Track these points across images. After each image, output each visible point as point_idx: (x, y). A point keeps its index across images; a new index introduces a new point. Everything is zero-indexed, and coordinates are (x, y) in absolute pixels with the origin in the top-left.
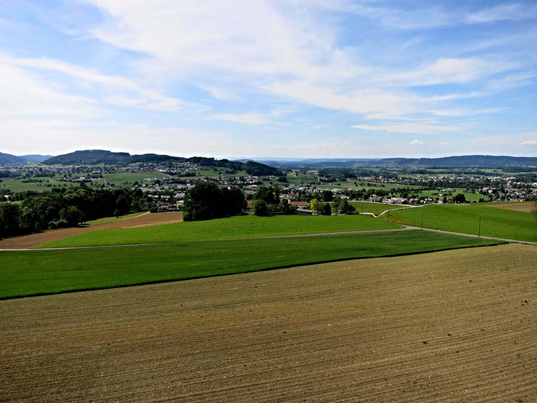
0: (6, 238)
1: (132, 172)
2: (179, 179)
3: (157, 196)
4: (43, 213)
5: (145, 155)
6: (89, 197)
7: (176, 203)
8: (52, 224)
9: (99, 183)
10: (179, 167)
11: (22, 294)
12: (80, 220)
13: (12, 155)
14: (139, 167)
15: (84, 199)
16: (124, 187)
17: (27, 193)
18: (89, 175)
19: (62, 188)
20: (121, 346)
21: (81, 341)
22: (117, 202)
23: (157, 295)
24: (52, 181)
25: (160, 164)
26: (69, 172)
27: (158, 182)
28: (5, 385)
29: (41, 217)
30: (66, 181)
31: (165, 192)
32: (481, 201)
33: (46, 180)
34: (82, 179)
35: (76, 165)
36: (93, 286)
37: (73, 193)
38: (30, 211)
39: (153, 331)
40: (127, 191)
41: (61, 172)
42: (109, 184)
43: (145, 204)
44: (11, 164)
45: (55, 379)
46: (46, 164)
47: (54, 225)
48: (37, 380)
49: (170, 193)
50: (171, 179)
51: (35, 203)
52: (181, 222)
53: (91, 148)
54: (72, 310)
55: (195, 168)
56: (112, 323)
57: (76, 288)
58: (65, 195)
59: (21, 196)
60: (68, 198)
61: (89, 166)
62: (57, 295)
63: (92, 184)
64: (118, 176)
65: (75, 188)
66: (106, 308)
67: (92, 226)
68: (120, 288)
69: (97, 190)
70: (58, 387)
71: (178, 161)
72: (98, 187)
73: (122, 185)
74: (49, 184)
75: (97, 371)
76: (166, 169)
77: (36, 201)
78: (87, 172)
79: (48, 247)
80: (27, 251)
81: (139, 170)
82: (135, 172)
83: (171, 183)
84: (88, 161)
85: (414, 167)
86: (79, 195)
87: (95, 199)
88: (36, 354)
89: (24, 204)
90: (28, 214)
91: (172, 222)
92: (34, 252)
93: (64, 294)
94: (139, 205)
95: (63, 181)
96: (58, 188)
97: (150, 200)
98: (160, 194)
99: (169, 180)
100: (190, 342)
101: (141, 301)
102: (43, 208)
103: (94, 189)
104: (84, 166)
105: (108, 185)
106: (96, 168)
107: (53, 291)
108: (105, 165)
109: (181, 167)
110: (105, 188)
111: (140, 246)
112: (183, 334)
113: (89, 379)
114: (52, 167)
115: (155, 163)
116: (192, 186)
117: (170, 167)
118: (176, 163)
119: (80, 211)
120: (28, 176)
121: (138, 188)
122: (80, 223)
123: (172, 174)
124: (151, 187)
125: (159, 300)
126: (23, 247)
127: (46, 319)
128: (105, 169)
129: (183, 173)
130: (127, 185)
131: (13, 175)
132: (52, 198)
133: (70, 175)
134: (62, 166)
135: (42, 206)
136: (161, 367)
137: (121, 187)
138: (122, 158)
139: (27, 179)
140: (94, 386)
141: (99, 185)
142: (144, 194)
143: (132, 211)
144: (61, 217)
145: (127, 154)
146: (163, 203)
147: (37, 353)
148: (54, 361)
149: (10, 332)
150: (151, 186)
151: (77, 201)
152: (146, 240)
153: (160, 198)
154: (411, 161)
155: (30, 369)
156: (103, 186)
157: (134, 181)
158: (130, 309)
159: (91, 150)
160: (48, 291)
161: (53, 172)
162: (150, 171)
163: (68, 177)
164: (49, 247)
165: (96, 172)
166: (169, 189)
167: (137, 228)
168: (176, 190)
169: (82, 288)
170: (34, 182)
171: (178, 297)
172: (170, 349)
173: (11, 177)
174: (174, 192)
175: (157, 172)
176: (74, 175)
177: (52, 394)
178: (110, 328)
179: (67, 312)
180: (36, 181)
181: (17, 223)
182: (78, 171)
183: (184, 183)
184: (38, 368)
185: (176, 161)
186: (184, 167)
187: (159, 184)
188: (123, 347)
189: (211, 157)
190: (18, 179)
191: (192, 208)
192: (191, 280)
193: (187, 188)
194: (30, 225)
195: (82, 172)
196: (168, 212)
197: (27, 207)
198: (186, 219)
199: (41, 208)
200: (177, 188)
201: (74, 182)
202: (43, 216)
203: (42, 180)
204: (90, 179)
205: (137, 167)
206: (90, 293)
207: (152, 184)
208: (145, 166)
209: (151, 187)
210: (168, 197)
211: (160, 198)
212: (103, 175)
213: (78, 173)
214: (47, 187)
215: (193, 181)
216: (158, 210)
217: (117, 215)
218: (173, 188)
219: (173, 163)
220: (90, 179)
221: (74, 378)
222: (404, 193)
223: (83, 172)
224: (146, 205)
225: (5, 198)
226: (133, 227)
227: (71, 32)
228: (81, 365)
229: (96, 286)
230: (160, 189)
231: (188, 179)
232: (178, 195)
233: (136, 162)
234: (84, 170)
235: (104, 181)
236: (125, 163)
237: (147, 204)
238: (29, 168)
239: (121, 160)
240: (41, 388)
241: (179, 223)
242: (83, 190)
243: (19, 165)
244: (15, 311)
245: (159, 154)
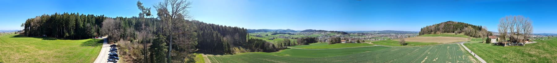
154: (376, 31)
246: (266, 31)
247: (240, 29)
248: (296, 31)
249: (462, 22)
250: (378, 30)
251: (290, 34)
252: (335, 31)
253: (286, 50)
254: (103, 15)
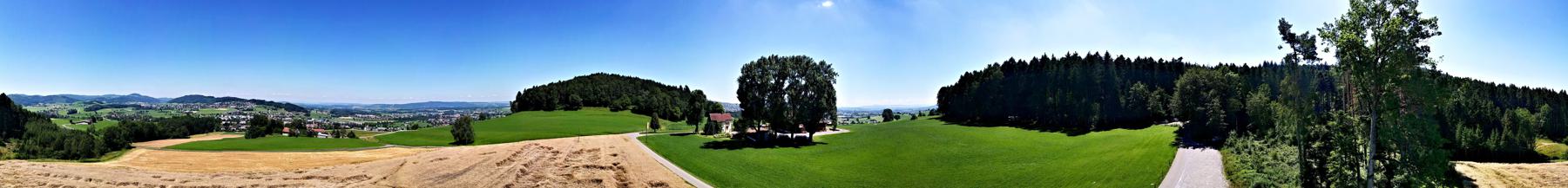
32: (428, 126)
55: (254, 106)
85: (390, 109)
154: (389, 106)
183: (246, 115)
222: (385, 125)
246: (69, 99)
247: (1554, 93)
248: (157, 101)
249: (633, 76)
250: (393, 103)
251: (139, 107)
252: (268, 100)
253: (805, 150)
254: (1181, 58)
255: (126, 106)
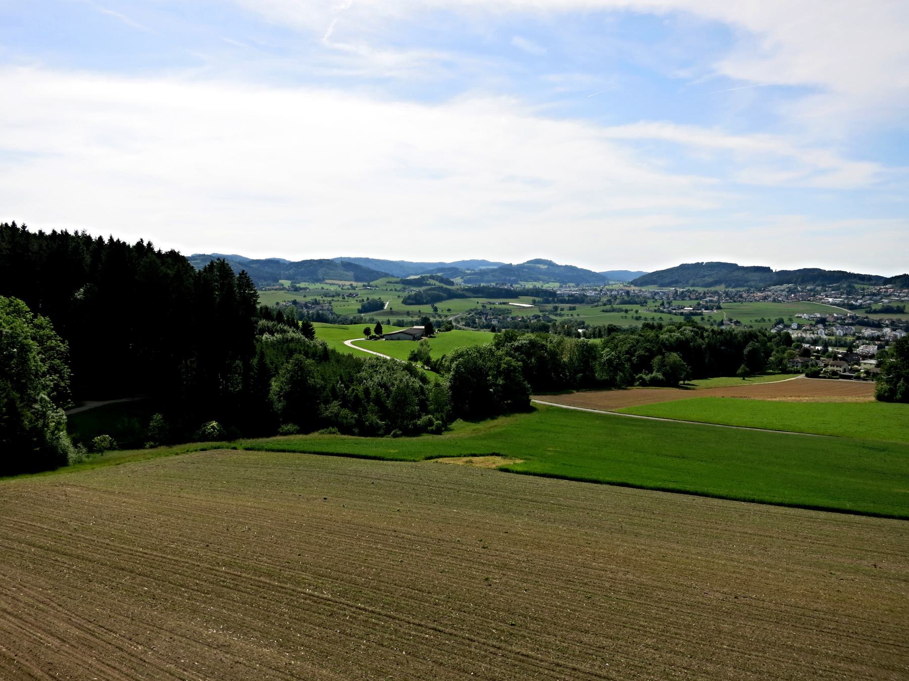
0: (578, 391)
1: (774, 301)
2: (867, 317)
3: (819, 348)
4: (629, 360)
5: (799, 271)
6: (700, 341)
7: (859, 364)
8: (641, 378)
9: (715, 318)
10: (869, 295)
11: (601, 478)
12: (682, 377)
13: (591, 271)
14: (788, 292)
15: (691, 344)
16: (756, 327)
17: (608, 328)
18: (699, 304)
19: (658, 324)
20: (758, 607)
21: (690, 578)
22: (746, 351)
23: (822, 532)
24: (643, 311)
25: (830, 287)
26: (668, 298)
27: (822, 321)
28: (582, 608)
29: (626, 366)
30: (662, 312)
31: (836, 341)
33: (634, 310)
34: (688, 309)
35: (680, 287)
36: (705, 490)
37: (674, 332)
38: (612, 356)
39: (818, 598)
40: (764, 335)
41: (657, 297)
42: (731, 320)
43: (795, 360)
44: (588, 284)
45: (651, 625)
46: (635, 285)
47: (644, 380)
48: (626, 617)
49: (845, 343)
50: (850, 317)
51: (619, 344)
52: (871, 402)
53: (705, 259)
54: (674, 521)
56: (739, 562)
57: (678, 488)
58: (662, 334)
59: (600, 331)
60: (667, 340)
61: (701, 290)
62: (649, 491)
63: (703, 319)
64: (747, 306)
65: (677, 325)
66: (729, 533)
67: (699, 389)
68: (752, 504)
69: (713, 331)
70: (655, 640)
71: (868, 283)
72: (712, 325)
73: (753, 323)
74: (638, 315)
75: (717, 637)
76: (840, 298)
77: (620, 341)
78: (697, 299)
79: (634, 413)
80: (605, 414)
81: (787, 298)
82: (780, 302)
83: (848, 324)
84: (698, 280)
86: (684, 335)
87: (709, 344)
88: (624, 577)
89: (603, 344)
90: (609, 360)
91: (850, 399)
92: (615, 417)
93: (661, 493)
94: (785, 361)
95: (658, 312)
96: (651, 323)
97: (807, 353)
98: (826, 345)
99: (845, 319)
100: (897, 644)
101: (790, 537)
102: (630, 352)
103: (707, 327)
104: (691, 289)
105: (729, 323)
106: (712, 293)
107: (645, 484)
108: (726, 288)
109: (874, 295)
110: (723, 327)
111: (786, 435)
112: (881, 623)
113: (704, 645)
114: (644, 289)
115: (818, 285)
116: (894, 333)
117: (849, 293)
118: (862, 286)
119: (685, 362)
120: (609, 302)
121: (782, 329)
122: (681, 382)
123: (852, 307)
124: (808, 330)
125: (827, 543)
126: (600, 407)
127: (634, 525)
128: (727, 294)
129: (879, 306)
130: (762, 323)
131: (590, 300)
132: (643, 338)
133: (669, 303)
134: (659, 288)
135: (629, 349)
136: (836, 673)
137: (751, 327)
138: (757, 276)
139: (608, 307)
140: (711, 659)
141: (715, 321)
142: (794, 342)
143: (771, 371)
144: (655, 369)
145: (767, 270)
146: (831, 362)
147: (625, 575)
148: (650, 596)
149: (587, 531)
150: (808, 327)
151: (681, 346)
152: (797, 425)
153: (825, 351)
155: (615, 596)
156: (722, 323)
157: (777, 318)
158: (771, 544)
159: (705, 262)
160: (638, 483)
161: (645, 297)
162: (809, 300)
163: (667, 306)
164: (636, 413)
165: (711, 298)
166: (845, 335)
167: (780, 402)
168: (859, 338)
169: (687, 489)
170: (618, 312)
171: (866, 547)
172: (853, 644)
173: (588, 303)
174: (854, 341)
175: (822, 303)
176: (675, 303)
177: (647, 647)
178: (738, 570)
179: (666, 523)
180: (620, 310)
181: (593, 371)
182: (683, 296)
183: (878, 325)
184: (625, 597)
185: (862, 282)
186: (879, 294)
187: (825, 325)
188: (762, 609)
189: (767, 266)
190: (597, 306)
191: (898, 377)
192: (895, 521)
193: (883, 336)
194: (610, 376)
195: (687, 299)
196: (841, 380)
197: (608, 349)
198: (880, 398)
199: (627, 352)
200: (861, 335)
201: (675, 314)
202: (629, 364)
203: (628, 309)
204: (700, 311)
205: (784, 293)
206: (700, 500)
207: (811, 324)
208: (798, 291)
209: (808, 330)
210: (842, 350)
211: (825, 351)
212: (722, 305)
213: (683, 300)
214: (634, 320)
215: (897, 323)
216: (820, 373)
217: (744, 375)
218: (854, 335)
219: (857, 286)
220: (700, 311)
221: (680, 634)
223: (691, 299)
224: (798, 362)
225: (579, 333)
226: (773, 399)
227: (682, 74)
228: (691, 617)
229: (711, 490)
230: (826, 335)
231: (886, 318)
232: (861, 349)
233: (781, 284)
234: (692, 297)
235: (723, 315)
236: (761, 285)
237: (800, 361)
238: (612, 290)
239: (754, 280)
240: (631, 631)
241: (865, 403)
242: (691, 328)
243: (599, 286)
244: (592, 501)
245: (827, 270)
251: (549, 296)
255: (514, 295)
